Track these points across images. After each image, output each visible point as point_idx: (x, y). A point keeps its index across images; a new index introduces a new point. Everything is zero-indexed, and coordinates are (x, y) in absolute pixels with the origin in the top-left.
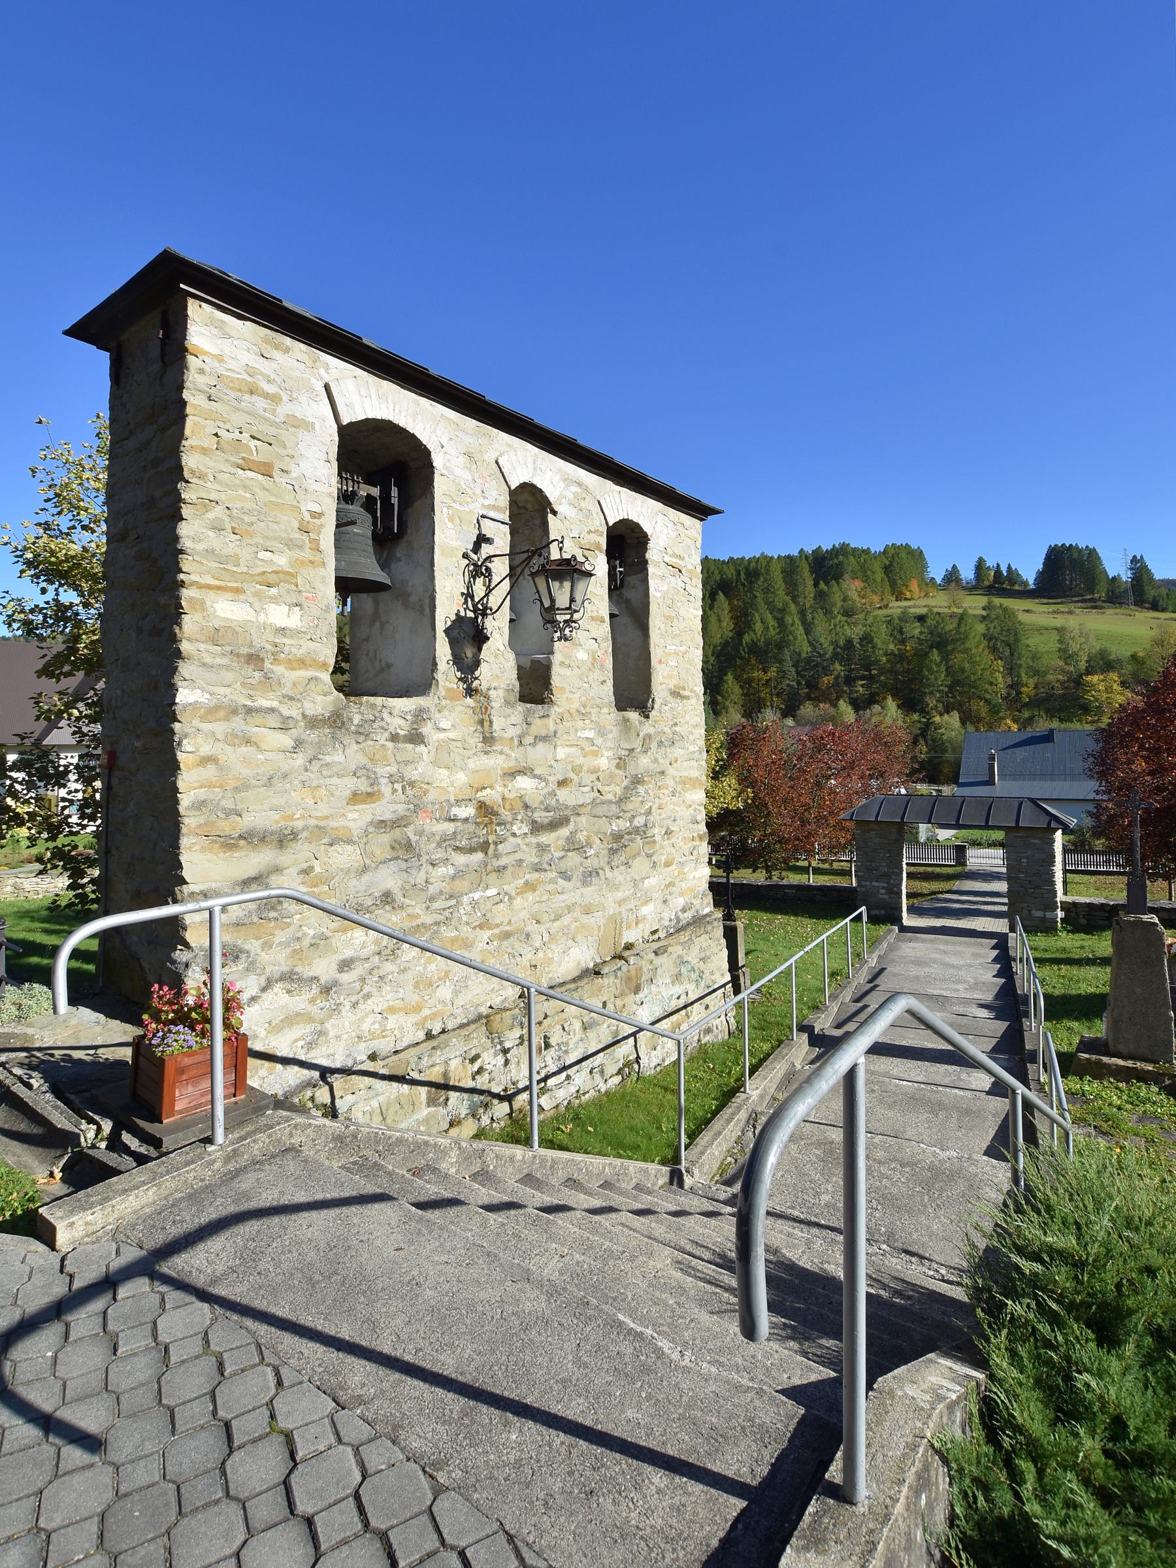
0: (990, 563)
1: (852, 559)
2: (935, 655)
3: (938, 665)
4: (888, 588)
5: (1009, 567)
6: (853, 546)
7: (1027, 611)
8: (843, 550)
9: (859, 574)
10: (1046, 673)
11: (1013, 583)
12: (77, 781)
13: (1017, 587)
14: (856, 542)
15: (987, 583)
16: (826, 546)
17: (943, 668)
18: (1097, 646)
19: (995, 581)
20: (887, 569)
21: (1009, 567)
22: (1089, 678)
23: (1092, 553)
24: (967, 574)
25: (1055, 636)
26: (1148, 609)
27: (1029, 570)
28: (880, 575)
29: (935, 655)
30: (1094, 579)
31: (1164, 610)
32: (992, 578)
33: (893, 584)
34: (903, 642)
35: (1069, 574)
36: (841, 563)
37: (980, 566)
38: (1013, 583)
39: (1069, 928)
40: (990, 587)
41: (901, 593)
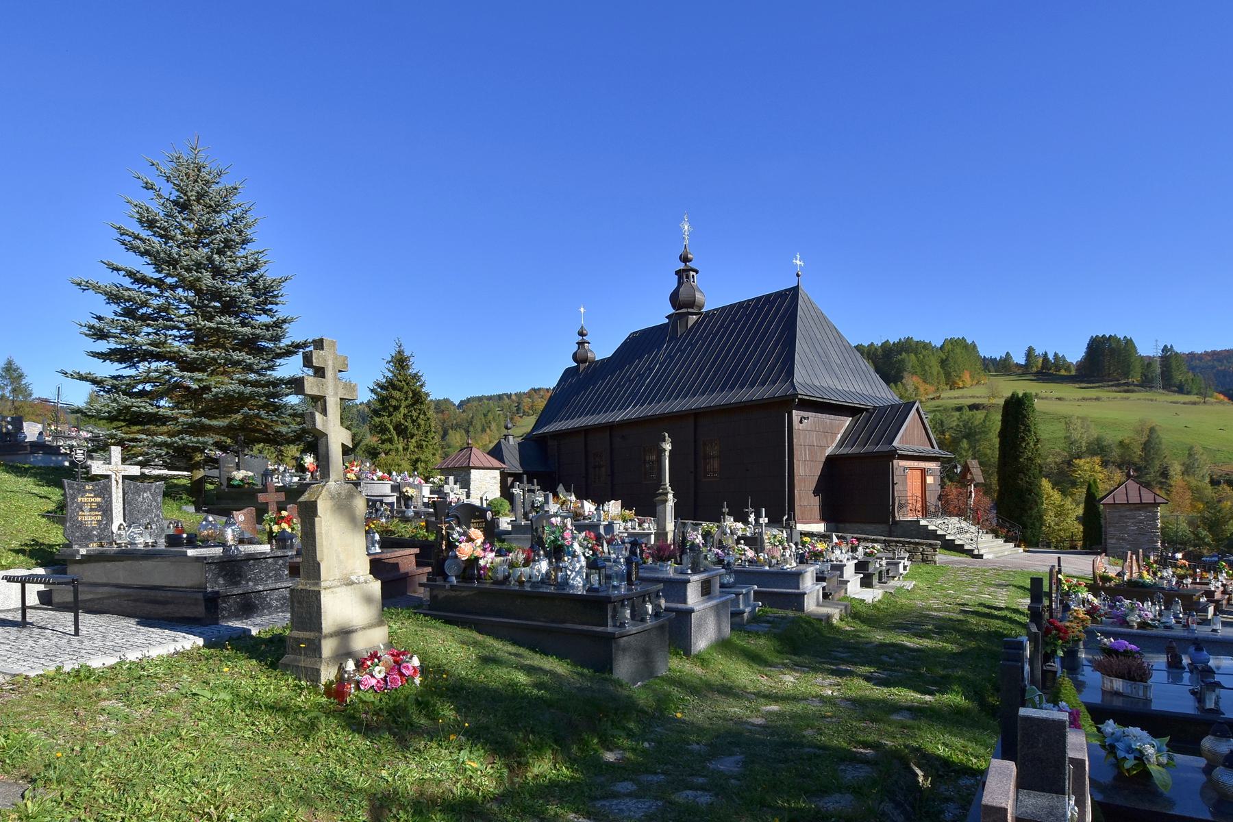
0: (1039, 351)
1: (912, 356)
2: (965, 444)
3: (967, 451)
4: (943, 379)
5: (1056, 355)
6: (915, 339)
7: (1059, 399)
8: (906, 346)
9: (919, 370)
10: (1047, 457)
11: (1058, 368)
12: (108, 461)
13: (1063, 372)
14: (919, 335)
15: (1035, 370)
16: (893, 339)
17: (970, 453)
18: (1095, 433)
19: (1043, 368)
20: (943, 363)
21: (1056, 355)
22: (1077, 461)
23: (1129, 342)
24: (1019, 359)
25: (1063, 426)
26: (1175, 392)
27: (1075, 354)
28: (936, 368)
29: (965, 444)
30: (1129, 366)
31: (1188, 393)
32: (1040, 365)
33: (948, 375)
34: (943, 433)
35: (1106, 363)
36: (903, 361)
37: (1030, 353)
38: (1058, 368)
39: (134, 409)
40: (1038, 373)
41: (954, 383)
